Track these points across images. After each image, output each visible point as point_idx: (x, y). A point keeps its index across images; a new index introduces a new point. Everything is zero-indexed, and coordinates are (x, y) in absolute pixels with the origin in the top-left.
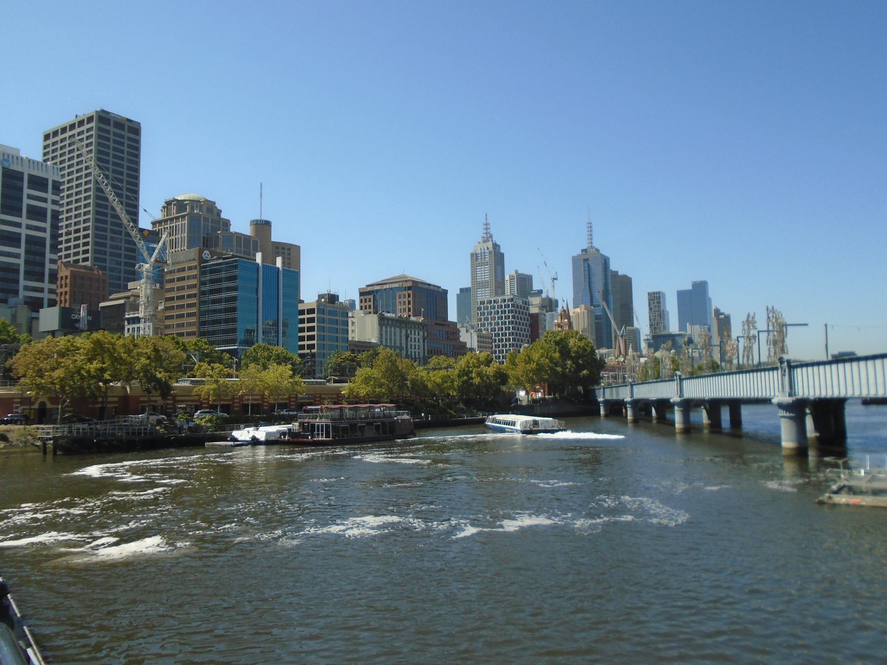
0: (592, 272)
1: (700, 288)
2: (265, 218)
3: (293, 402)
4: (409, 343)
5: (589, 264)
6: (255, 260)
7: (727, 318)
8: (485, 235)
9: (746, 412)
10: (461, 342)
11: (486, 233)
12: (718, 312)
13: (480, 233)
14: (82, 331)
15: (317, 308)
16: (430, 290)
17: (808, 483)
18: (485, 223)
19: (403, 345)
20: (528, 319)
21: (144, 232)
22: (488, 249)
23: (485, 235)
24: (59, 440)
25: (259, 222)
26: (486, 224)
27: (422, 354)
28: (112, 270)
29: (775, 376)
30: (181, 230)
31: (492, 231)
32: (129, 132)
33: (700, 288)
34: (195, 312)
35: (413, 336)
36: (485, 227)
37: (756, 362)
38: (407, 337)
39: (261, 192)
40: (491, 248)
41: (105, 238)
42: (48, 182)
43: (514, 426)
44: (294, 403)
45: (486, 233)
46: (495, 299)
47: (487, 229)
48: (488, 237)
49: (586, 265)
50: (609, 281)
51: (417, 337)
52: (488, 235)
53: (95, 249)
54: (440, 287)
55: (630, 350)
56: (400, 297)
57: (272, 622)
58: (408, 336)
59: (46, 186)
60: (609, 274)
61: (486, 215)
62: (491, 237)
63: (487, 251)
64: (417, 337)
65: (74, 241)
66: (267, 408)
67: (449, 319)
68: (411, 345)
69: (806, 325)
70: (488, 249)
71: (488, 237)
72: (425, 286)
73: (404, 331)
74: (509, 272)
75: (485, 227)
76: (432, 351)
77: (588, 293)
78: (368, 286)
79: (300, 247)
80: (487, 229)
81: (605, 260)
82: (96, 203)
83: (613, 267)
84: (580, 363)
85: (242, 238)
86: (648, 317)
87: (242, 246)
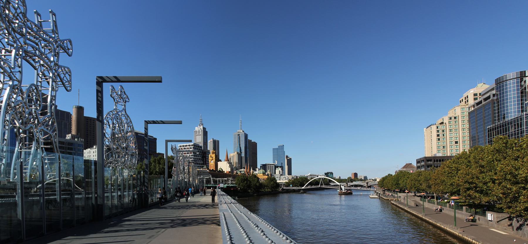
2: (80, 105)
5: (240, 136)
6: (479, 84)
7: (291, 159)
9: (218, 209)
10: (83, 151)
17: (168, 184)
20: (201, 154)
22: (201, 129)
29: (20, 40)
32: (497, 130)
40: (202, 128)
43: (439, 136)
49: (239, 137)
50: (247, 143)
54: (153, 137)
55: (251, 170)
57: (356, 186)
59: (518, 123)
60: (247, 140)
63: (200, 130)
67: (158, 151)
69: (180, 123)
70: (201, 129)
72: (90, 174)
77: (67, 55)
79: (156, 138)
81: (246, 135)
82: (67, 199)
83: (249, 138)
84: (516, 240)
85: (60, 112)
86: (495, 82)
87: (60, 115)
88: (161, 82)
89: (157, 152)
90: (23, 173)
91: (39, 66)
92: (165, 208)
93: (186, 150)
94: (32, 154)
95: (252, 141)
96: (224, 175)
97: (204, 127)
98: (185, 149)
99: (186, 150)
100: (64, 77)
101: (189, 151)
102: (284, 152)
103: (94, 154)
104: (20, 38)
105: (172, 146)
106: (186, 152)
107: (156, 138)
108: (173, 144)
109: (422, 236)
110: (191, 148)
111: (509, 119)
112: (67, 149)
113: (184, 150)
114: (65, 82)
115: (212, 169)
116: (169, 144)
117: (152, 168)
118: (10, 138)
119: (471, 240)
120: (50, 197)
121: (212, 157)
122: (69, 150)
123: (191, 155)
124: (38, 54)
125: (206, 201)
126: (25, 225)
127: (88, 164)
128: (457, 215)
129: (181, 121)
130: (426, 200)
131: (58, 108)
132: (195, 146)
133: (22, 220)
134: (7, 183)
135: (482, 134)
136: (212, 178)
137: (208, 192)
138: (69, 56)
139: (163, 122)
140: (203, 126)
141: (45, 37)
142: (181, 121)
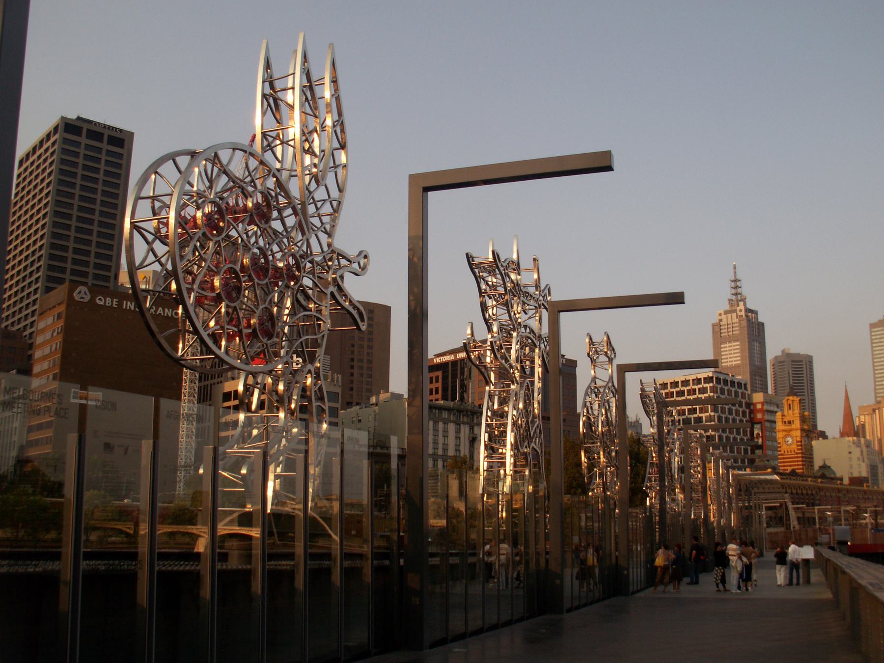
0: (468, 496)
11: (736, 294)
13: (727, 293)
14: (876, 520)
15: (751, 382)
16: (515, 472)
18: (733, 278)
20: (744, 413)
23: (734, 298)
24: (248, 382)
26: (735, 281)
30: (207, 389)
31: (745, 291)
36: (733, 284)
40: (743, 313)
45: (736, 294)
47: (736, 287)
48: (738, 297)
53: (48, 276)
61: (735, 268)
62: (744, 300)
69: (676, 299)
71: (738, 297)
74: (773, 350)
75: (733, 284)
80: (736, 287)
90: (220, 469)
91: (141, 266)
93: (683, 398)
96: (839, 491)
97: (199, 188)
98: (692, 392)
99: (683, 398)
100: (154, 241)
101: (698, 401)
102: (641, 424)
103: (434, 386)
105: (642, 384)
106: (683, 408)
107: (610, 152)
108: (648, 377)
109: (652, 473)
110: (703, 391)
112: (250, 361)
113: (679, 399)
114: (319, 206)
115: (789, 469)
116: (629, 376)
117: (632, 434)
118: (77, 447)
121: (789, 422)
125: (71, 598)
128: (278, 147)
129: (608, 154)
130: (441, 518)
132: (718, 380)
133: (211, 601)
135: (437, 389)
136: (791, 506)
137: (873, 428)
138: (472, 323)
140: (745, 305)
142: (608, 154)
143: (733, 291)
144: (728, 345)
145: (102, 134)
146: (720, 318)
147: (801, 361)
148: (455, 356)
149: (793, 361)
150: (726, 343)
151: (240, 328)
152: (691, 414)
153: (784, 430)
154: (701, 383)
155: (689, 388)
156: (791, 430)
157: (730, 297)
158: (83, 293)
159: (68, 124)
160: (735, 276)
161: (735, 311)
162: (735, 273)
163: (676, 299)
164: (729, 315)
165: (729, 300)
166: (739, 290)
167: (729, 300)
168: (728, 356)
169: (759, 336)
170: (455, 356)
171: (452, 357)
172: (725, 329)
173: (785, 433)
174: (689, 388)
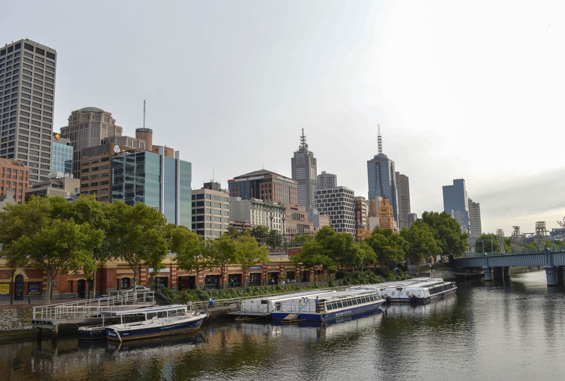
1: (459, 183)
3: (144, 277)
4: (273, 223)
8: (302, 145)
11: (303, 144)
12: (470, 201)
18: (302, 136)
19: (269, 226)
21: (56, 136)
23: (302, 145)
25: (143, 130)
26: (303, 137)
27: (283, 233)
28: (31, 164)
31: (307, 142)
33: (459, 183)
34: (108, 181)
35: (275, 218)
36: (302, 139)
37: (384, 188)
38: (271, 218)
39: (145, 104)
41: (27, 139)
42: (3, 144)
44: (145, 279)
45: (303, 144)
46: (328, 189)
49: (378, 167)
51: (278, 218)
52: (305, 145)
54: (352, 193)
56: (262, 187)
58: (273, 218)
60: (394, 174)
61: (303, 130)
64: (278, 218)
65: (9, 152)
66: (202, 281)
68: (274, 225)
69: (145, 101)
73: (269, 214)
75: (302, 139)
76: (289, 229)
78: (236, 178)
80: (303, 140)
88: (4, 168)
89: (453, 184)
92: (284, 363)
94: (200, 346)
95: (400, 174)
104: (126, 283)
111: (125, 300)
119: (432, 287)
120: (503, 277)
122: (216, 207)
123: (326, 204)
124: (286, 258)
126: (127, 143)
127: (316, 212)
131: (203, 187)
134: (431, 294)
139: (144, 111)
141: (24, 365)
143: (302, 142)
144: (299, 169)
145: (33, 47)
146: (295, 155)
147: (331, 178)
148: (248, 179)
149: (327, 178)
150: (298, 168)
151: (233, 179)
152: (327, 206)
153: (382, 214)
154: (326, 193)
155: (331, 194)
156: (386, 214)
157: (300, 145)
158: (117, 148)
159: (192, 220)
160: (303, 135)
161: (303, 152)
162: (303, 133)
163: (145, 101)
164: (300, 154)
165: (300, 146)
166: (305, 142)
167: (300, 146)
168: (299, 175)
169: (314, 165)
170: (248, 179)
171: (246, 179)
172: (298, 161)
173: (383, 215)
174: (331, 194)
